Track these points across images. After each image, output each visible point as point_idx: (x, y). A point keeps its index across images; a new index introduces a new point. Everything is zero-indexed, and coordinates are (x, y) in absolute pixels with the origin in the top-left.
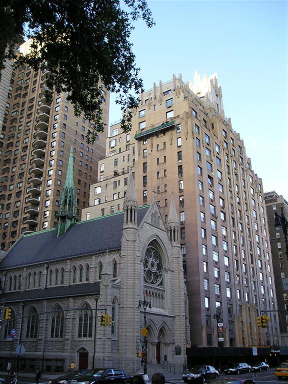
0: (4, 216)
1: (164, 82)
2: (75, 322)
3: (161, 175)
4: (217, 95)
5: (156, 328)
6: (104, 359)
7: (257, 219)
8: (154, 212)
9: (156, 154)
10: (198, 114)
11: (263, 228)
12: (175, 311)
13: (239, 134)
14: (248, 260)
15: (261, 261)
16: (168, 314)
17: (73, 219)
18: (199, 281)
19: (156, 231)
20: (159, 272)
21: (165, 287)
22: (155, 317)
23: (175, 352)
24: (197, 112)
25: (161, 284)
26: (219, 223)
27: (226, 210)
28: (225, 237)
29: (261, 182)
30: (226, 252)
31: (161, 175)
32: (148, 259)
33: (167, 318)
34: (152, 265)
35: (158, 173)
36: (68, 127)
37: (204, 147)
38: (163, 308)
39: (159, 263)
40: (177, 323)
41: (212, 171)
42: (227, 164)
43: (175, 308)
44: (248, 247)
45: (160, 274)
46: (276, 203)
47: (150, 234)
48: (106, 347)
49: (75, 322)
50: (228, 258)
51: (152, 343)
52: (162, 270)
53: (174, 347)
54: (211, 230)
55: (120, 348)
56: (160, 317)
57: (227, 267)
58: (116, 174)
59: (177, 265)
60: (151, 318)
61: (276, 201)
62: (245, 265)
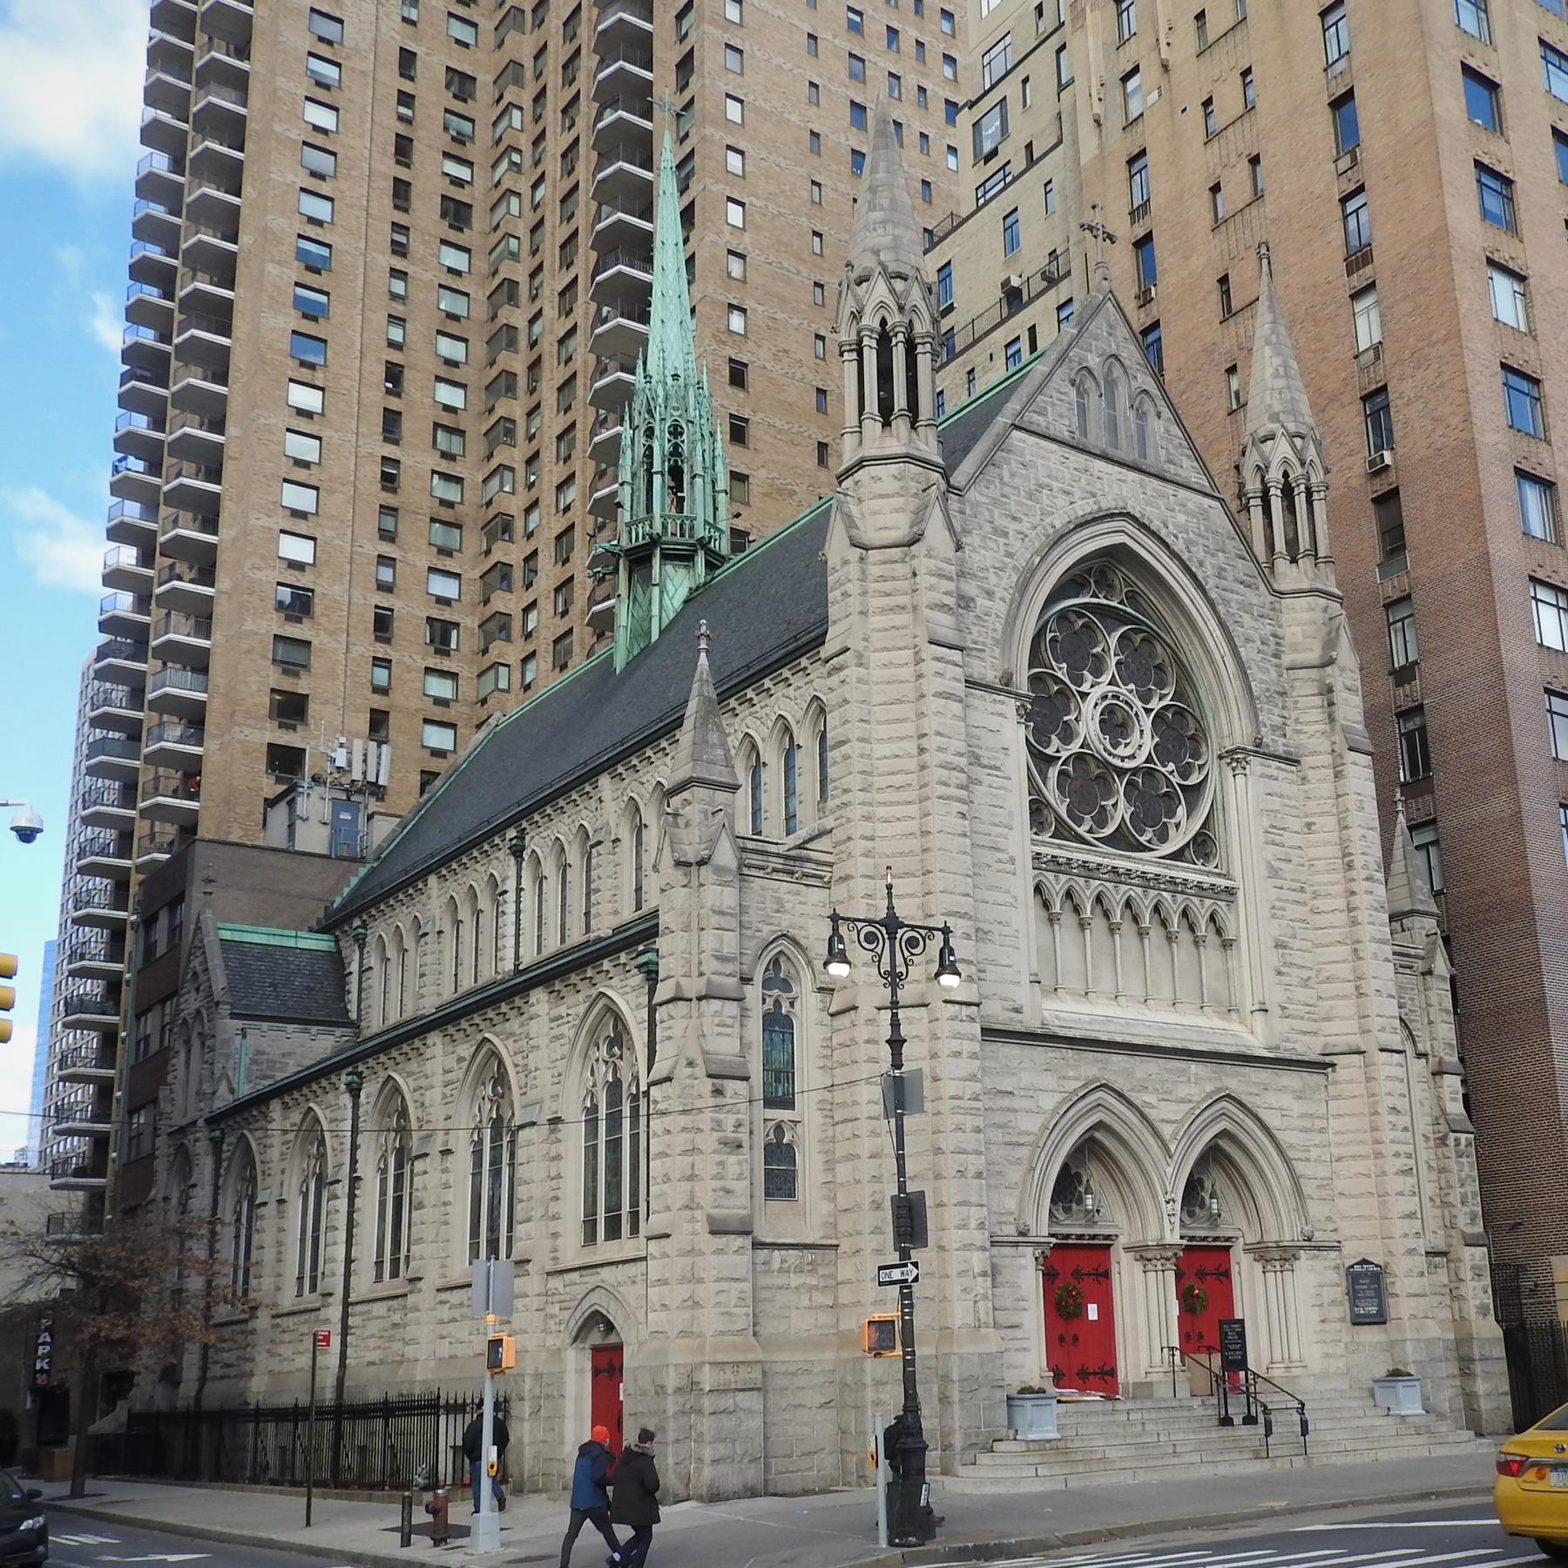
0: (517, 675)
2: (561, 1148)
3: (1236, 191)
6: (691, 1386)
17: (700, 559)
18: (1517, 817)
19: (1120, 487)
20: (1185, 772)
21: (1236, 870)
25: (1203, 846)
31: (1236, 191)
34: (1115, 723)
35: (1216, 189)
36: (758, 110)
39: (1180, 713)
45: (1194, 779)
48: (704, 1292)
49: (561, 1148)
51: (1141, 1253)
52: (1210, 754)
55: (845, 1296)
58: (1014, 298)
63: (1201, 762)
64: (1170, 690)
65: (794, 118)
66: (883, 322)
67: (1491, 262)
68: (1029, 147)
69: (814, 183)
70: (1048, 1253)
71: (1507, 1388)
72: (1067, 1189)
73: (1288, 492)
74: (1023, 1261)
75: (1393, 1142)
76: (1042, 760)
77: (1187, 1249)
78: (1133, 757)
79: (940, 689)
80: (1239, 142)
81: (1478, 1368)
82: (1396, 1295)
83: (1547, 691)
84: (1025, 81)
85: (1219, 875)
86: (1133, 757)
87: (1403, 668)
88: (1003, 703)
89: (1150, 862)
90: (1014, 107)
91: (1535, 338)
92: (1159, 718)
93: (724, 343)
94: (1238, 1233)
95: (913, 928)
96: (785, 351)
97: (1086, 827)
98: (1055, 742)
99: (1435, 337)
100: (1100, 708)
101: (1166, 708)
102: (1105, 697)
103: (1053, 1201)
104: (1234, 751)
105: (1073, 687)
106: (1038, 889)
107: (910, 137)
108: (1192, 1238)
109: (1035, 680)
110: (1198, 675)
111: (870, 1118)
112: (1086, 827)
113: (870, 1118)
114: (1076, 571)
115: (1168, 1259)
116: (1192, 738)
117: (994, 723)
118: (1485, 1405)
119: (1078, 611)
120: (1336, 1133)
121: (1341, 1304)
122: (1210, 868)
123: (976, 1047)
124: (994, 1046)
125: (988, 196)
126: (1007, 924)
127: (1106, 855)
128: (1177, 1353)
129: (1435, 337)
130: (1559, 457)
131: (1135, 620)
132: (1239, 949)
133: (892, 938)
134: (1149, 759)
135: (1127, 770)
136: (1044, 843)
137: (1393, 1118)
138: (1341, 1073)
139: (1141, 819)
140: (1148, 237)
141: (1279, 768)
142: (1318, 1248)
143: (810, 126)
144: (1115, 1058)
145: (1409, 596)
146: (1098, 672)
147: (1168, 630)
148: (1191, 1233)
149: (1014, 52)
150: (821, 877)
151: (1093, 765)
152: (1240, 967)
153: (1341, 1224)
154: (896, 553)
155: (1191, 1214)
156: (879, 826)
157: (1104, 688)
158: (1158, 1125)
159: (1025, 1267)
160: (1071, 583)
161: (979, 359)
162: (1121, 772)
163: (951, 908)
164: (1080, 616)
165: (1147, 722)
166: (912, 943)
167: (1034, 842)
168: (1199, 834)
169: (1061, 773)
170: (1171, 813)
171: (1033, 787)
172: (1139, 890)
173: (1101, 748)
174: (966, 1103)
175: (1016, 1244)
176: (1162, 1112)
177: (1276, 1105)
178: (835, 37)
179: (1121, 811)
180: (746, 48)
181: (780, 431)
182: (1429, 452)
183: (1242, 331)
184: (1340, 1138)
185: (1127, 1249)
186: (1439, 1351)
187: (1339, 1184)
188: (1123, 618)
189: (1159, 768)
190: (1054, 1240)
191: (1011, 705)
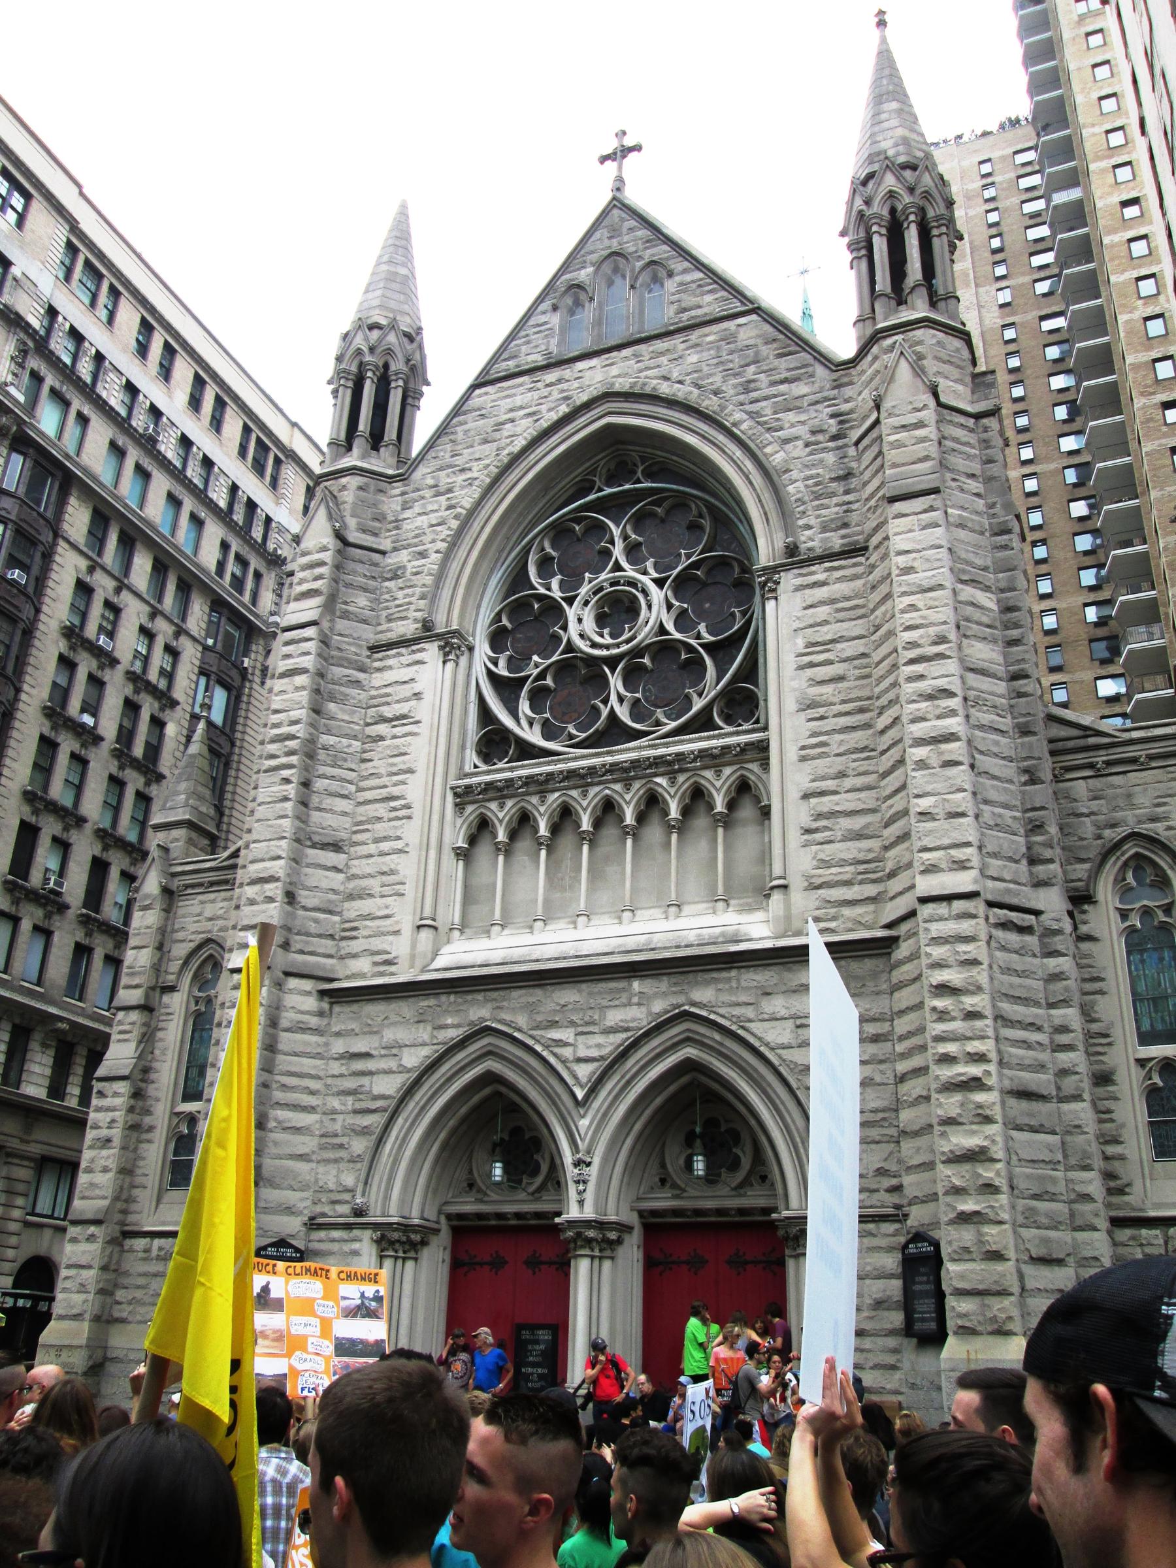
88: (423, 650)
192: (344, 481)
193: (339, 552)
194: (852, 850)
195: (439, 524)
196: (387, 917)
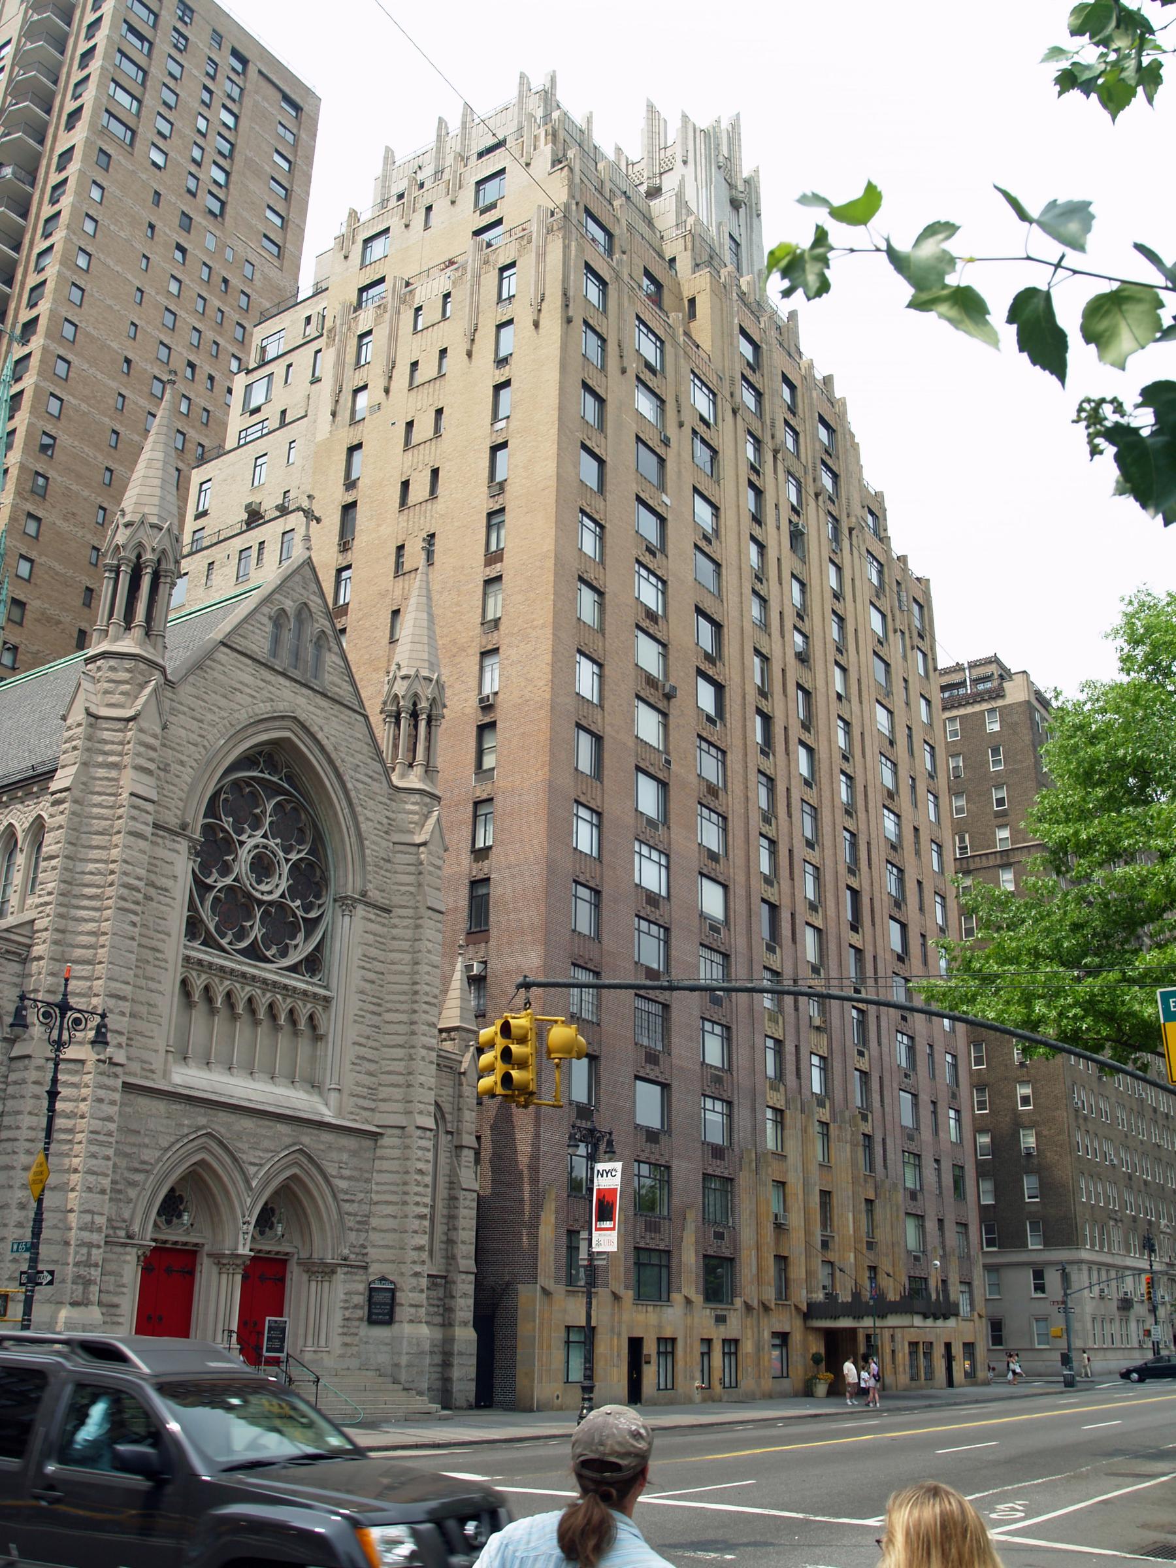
1: (482, 109)
4: (735, 204)
5: (247, 1182)
7: (892, 743)
8: (289, 605)
9: (403, 404)
10: (616, 242)
11: (921, 787)
12: (383, 1106)
13: (828, 380)
14: (831, 912)
15: (904, 927)
16: (339, 1114)
20: (307, 908)
21: (334, 985)
22: (248, 1123)
23: (362, 1313)
24: (616, 231)
25: (312, 964)
26: (685, 726)
27: (729, 673)
28: (712, 790)
29: (927, 593)
30: (713, 856)
32: (240, 832)
33: (327, 1137)
34: (262, 866)
36: (88, 334)
37: (624, 371)
38: (315, 1086)
39: (311, 865)
40: (386, 1165)
41: (662, 487)
42: (754, 478)
43: (384, 1092)
44: (835, 854)
45: (313, 915)
46: (1000, 703)
47: (246, 708)
50: (725, 887)
52: (327, 899)
53: (361, 1287)
54: (631, 743)
56: (282, 1128)
57: (714, 929)
58: (254, 517)
59: (411, 879)
60: (221, 1130)
61: (999, 694)
62: (818, 931)
63: (320, 902)
64: (306, 848)
65: (114, 345)
66: (139, 557)
67: (581, 579)
68: (284, 412)
69: (120, 394)
70: (148, 1253)
71: (474, 1376)
72: (171, 1207)
73: (414, 715)
74: (128, 1258)
75: (416, 1194)
76: (202, 887)
77: (253, 1257)
78: (270, 892)
79: (133, 829)
80: (428, 456)
81: (456, 1361)
82: (402, 1305)
83: (575, 881)
84: (289, 366)
85: (320, 986)
86: (270, 892)
87: (481, 850)
88: (178, 842)
89: (270, 971)
90: (278, 380)
91: (603, 635)
92: (295, 867)
93: (26, 500)
94: (295, 1250)
95: (79, 1011)
96: (74, 514)
97: (227, 940)
98: (215, 875)
99: (535, 623)
100: (252, 854)
101: (301, 859)
102: (257, 846)
103: (159, 1214)
104: (346, 898)
105: (234, 836)
106: (184, 982)
107: (201, 375)
108: (260, 1251)
109: (207, 829)
110: (327, 838)
111: (27, 1140)
112: (227, 940)
113: (27, 1140)
114: (251, 752)
115: (237, 1265)
116: (317, 884)
117: (169, 855)
118: (456, 1387)
119: (248, 782)
120: (377, 1184)
121: (362, 1308)
122: (315, 980)
123: (117, 1096)
124: (132, 1097)
125: (248, 439)
126: (155, 1006)
127: (240, 963)
128: (235, 1336)
129: (535, 623)
130: (608, 719)
131: (287, 793)
132: (327, 1042)
133: (63, 1017)
134: (282, 896)
135: (264, 902)
136: (193, 949)
137: (418, 1177)
138: (385, 1141)
139: (268, 940)
140: (353, 505)
141: (378, 915)
142: (351, 1266)
143: (126, 353)
144: (221, 1114)
145: (491, 799)
146: (256, 826)
147: (311, 804)
148: (258, 1247)
149: (285, 344)
150: (20, 955)
151: (240, 895)
152: (326, 1055)
153: (369, 1250)
154: (120, 725)
155: (262, 1233)
156: (71, 923)
157: (258, 840)
158: (245, 1166)
159: (129, 1262)
160: (247, 760)
161: (219, 556)
162: (260, 903)
163: (114, 992)
164: (249, 785)
165: (286, 868)
166: (77, 1022)
167: (186, 947)
168: (310, 954)
169: (215, 898)
170: (293, 937)
171: (192, 906)
172: (259, 991)
173: (248, 883)
174: (101, 1138)
175: (125, 1245)
176: (248, 1156)
177: (336, 1159)
178: (157, 293)
179: (257, 932)
180: (87, 288)
181: (57, 573)
182: (520, 701)
183: (406, 587)
184: (380, 1188)
185: (209, 1255)
186: (427, 1347)
187: (374, 1222)
188: (279, 791)
189: (289, 903)
190: (153, 1244)
191: (183, 846)
192: (98, 663)
193: (91, 725)
194: (369, 1080)
195: (194, 745)
196: (152, 1038)
